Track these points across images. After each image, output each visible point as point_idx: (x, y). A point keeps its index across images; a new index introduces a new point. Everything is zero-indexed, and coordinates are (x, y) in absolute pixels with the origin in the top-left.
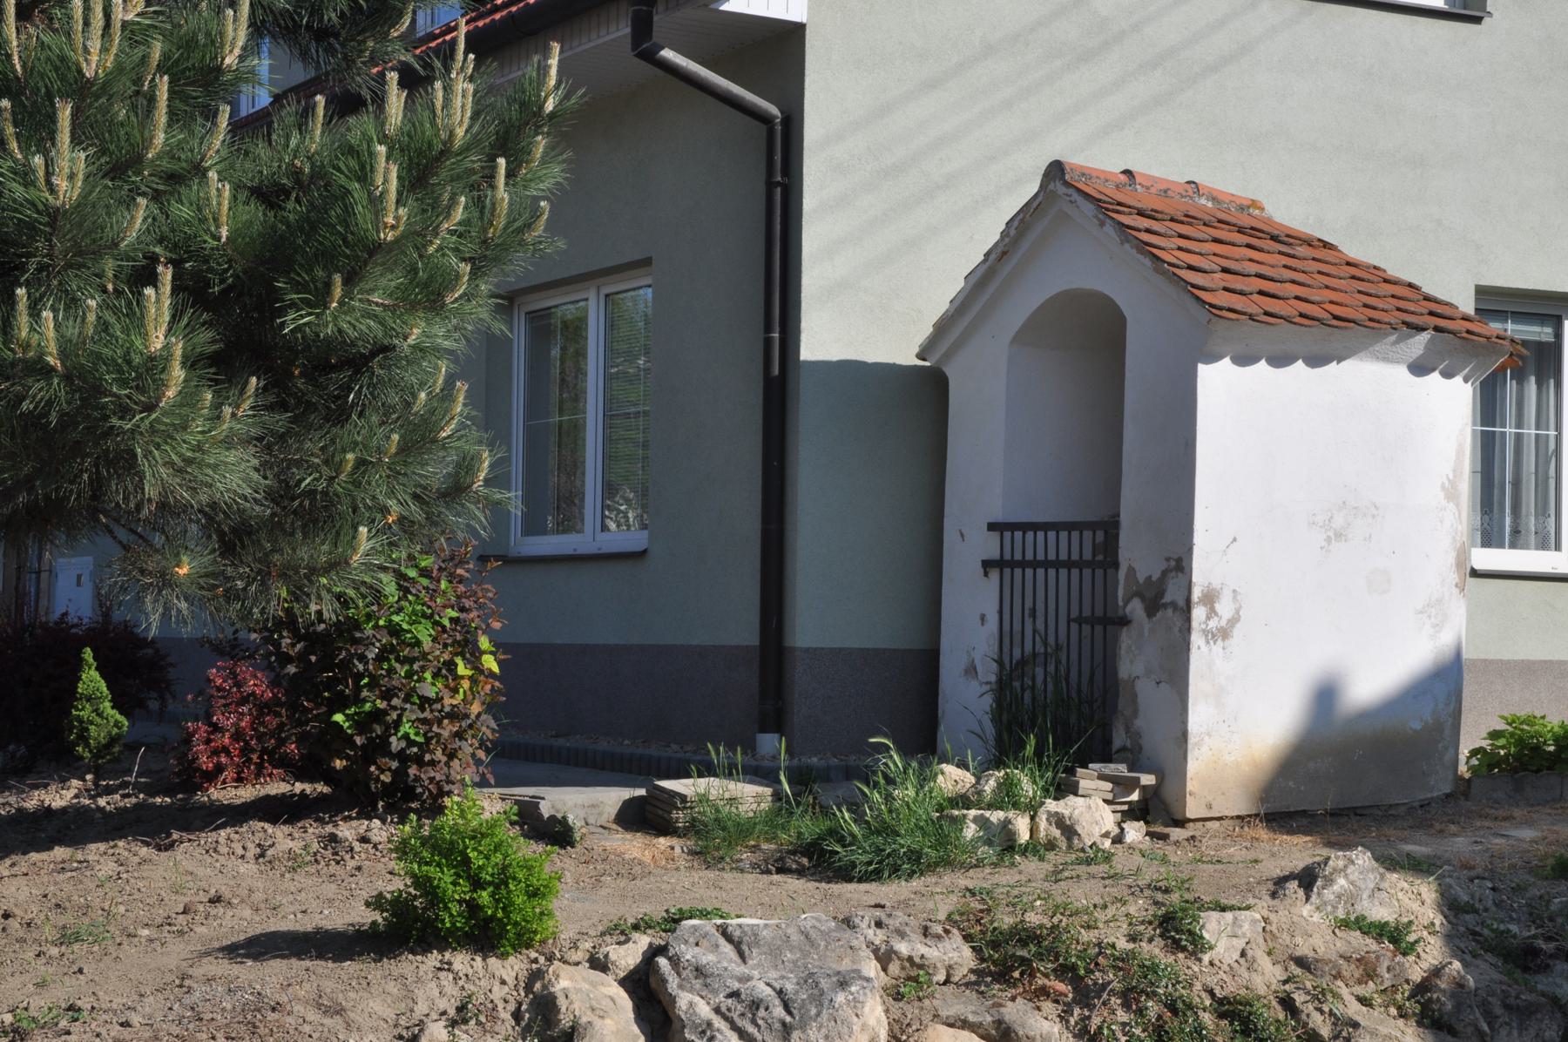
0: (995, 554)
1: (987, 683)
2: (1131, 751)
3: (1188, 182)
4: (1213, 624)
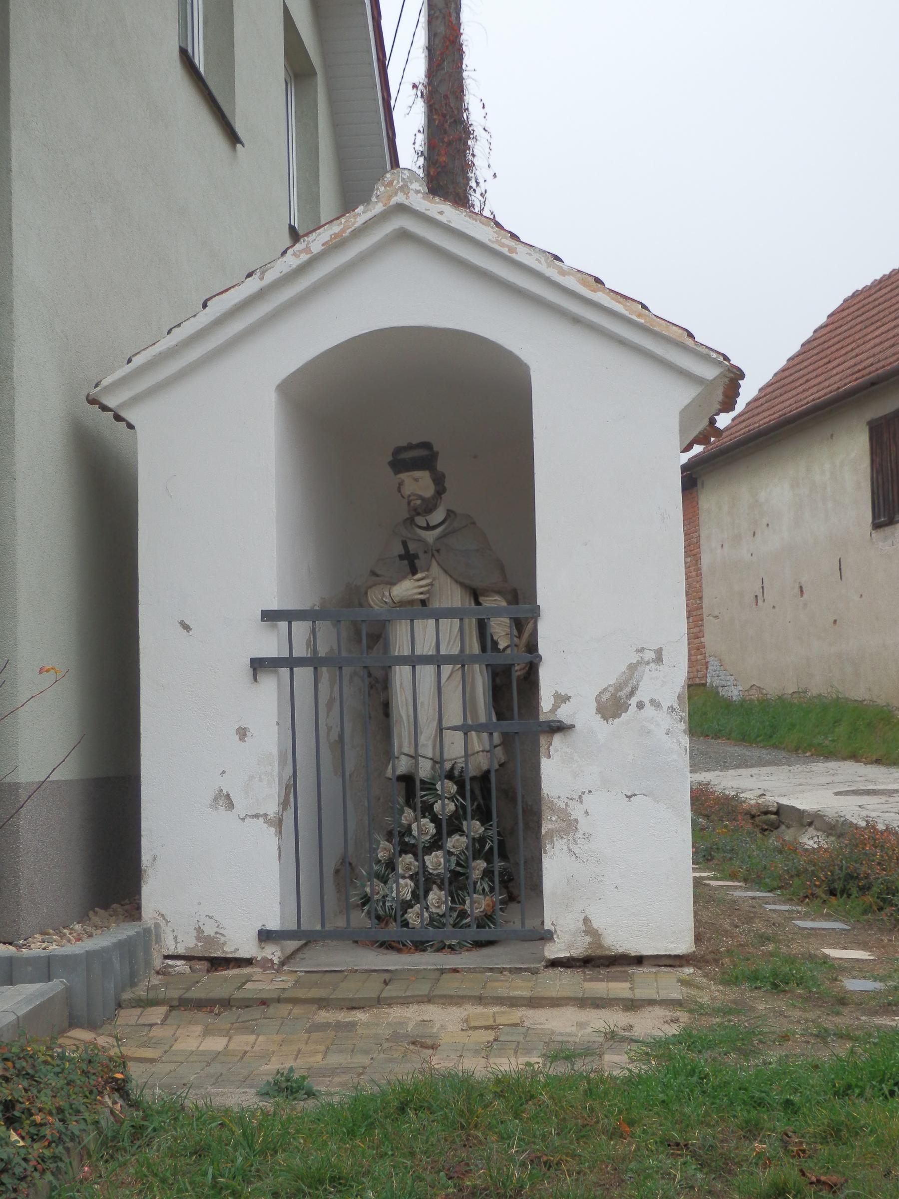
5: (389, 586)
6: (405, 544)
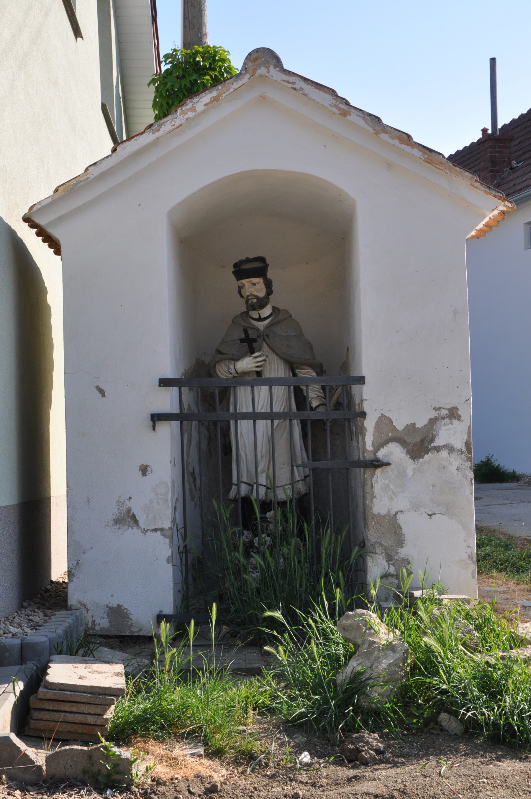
5: (233, 362)
6: (245, 331)
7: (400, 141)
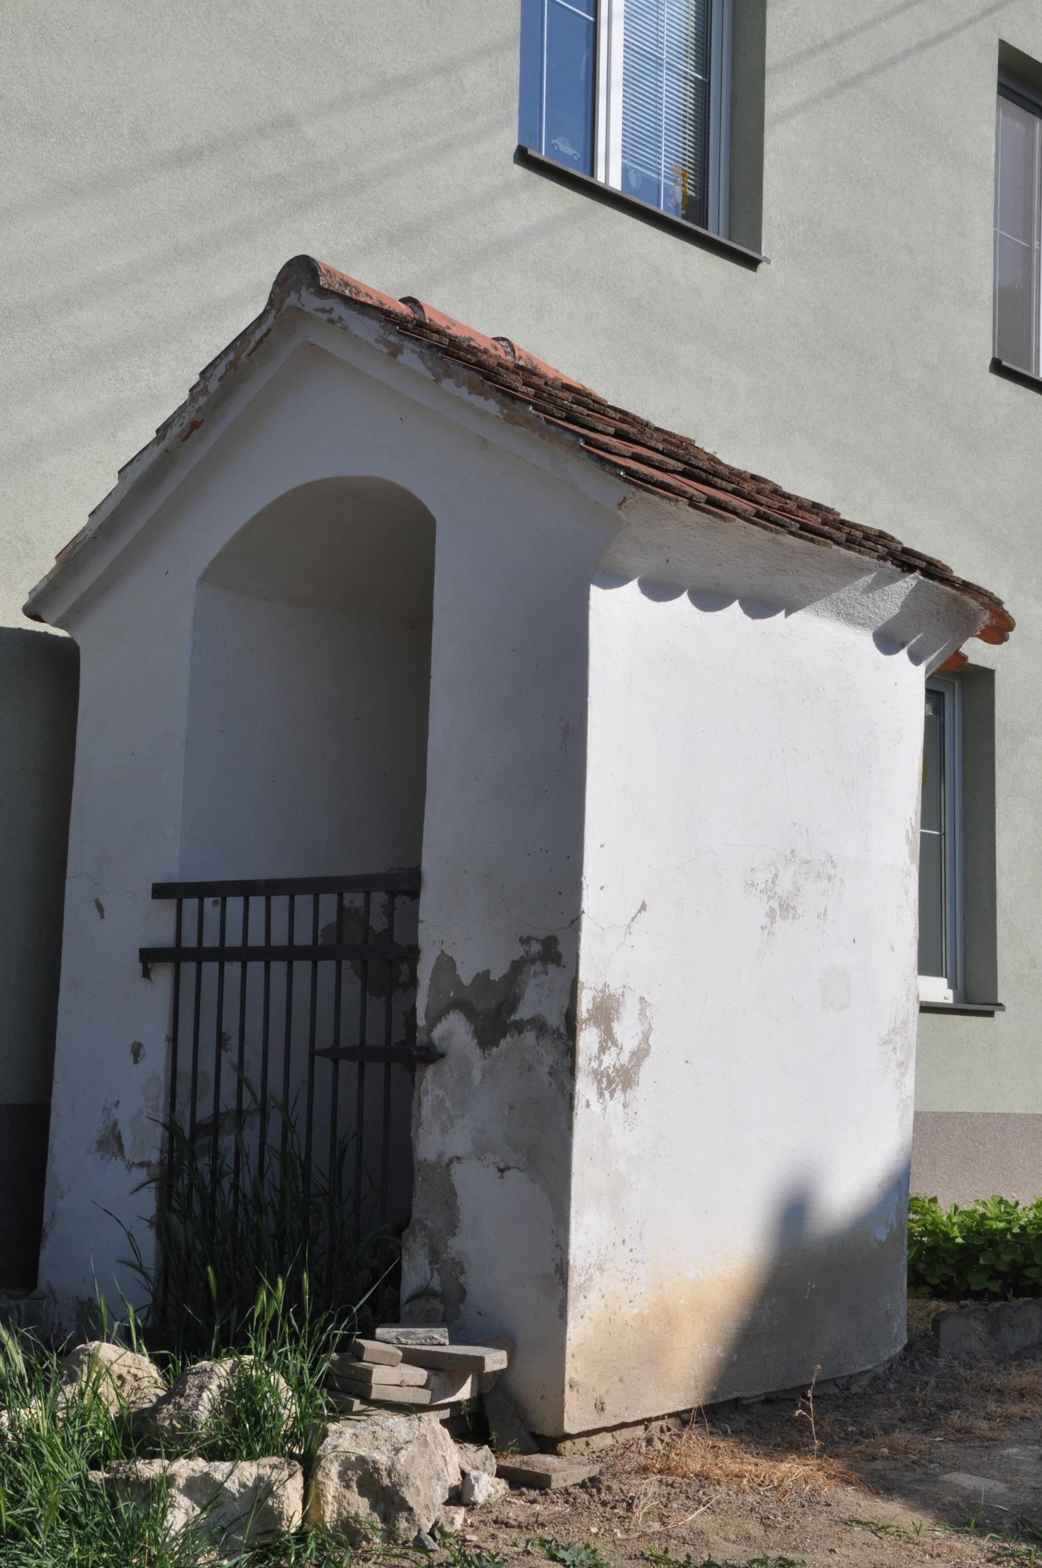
0: (163, 936)
1: (141, 1165)
2: (442, 1297)
3: (497, 339)
4: (609, 1060)
7: (469, 389)
